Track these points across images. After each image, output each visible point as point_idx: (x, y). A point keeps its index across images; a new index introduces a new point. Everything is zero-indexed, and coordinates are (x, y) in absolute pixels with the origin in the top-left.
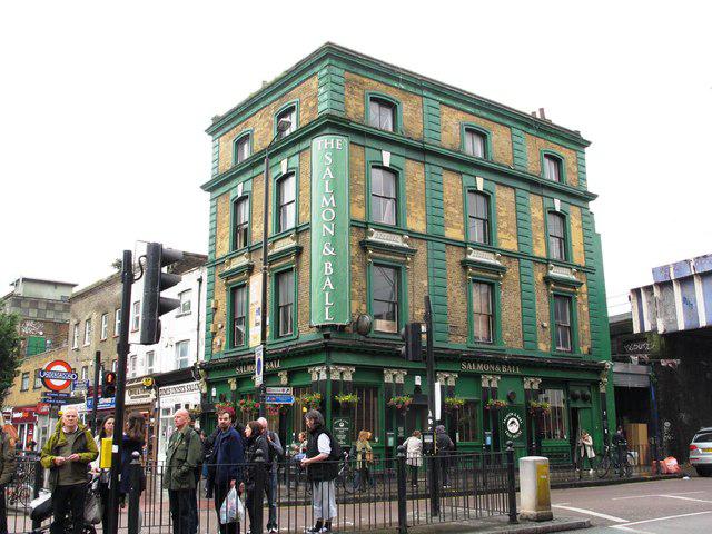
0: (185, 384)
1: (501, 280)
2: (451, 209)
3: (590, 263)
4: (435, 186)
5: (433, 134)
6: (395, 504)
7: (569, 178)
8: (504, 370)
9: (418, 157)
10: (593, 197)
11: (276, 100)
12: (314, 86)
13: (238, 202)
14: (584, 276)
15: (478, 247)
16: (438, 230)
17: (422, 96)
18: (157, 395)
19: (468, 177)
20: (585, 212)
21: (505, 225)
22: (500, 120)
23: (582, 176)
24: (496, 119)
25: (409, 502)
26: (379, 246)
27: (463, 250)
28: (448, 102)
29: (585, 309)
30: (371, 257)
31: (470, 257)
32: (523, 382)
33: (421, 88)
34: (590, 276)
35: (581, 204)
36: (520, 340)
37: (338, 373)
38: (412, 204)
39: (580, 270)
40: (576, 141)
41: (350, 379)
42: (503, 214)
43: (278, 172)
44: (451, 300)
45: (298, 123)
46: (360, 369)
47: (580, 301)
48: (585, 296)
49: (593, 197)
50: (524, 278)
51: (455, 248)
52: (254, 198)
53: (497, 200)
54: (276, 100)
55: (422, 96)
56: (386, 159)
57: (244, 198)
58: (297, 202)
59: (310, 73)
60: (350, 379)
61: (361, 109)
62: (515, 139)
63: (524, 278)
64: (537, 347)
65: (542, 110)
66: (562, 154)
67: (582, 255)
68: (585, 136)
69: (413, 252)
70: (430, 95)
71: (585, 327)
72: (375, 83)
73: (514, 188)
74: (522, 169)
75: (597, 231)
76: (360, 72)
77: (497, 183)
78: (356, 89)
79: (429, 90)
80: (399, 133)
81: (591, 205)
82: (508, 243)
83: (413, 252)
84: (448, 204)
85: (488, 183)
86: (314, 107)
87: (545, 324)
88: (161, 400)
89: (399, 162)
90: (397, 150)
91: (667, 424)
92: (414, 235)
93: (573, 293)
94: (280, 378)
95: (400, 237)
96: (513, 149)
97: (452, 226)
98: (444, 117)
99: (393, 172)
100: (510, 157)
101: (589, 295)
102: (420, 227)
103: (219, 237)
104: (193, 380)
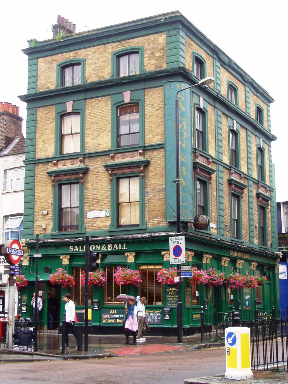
32: (250, 265)
40: (268, 100)
103: (38, 139)
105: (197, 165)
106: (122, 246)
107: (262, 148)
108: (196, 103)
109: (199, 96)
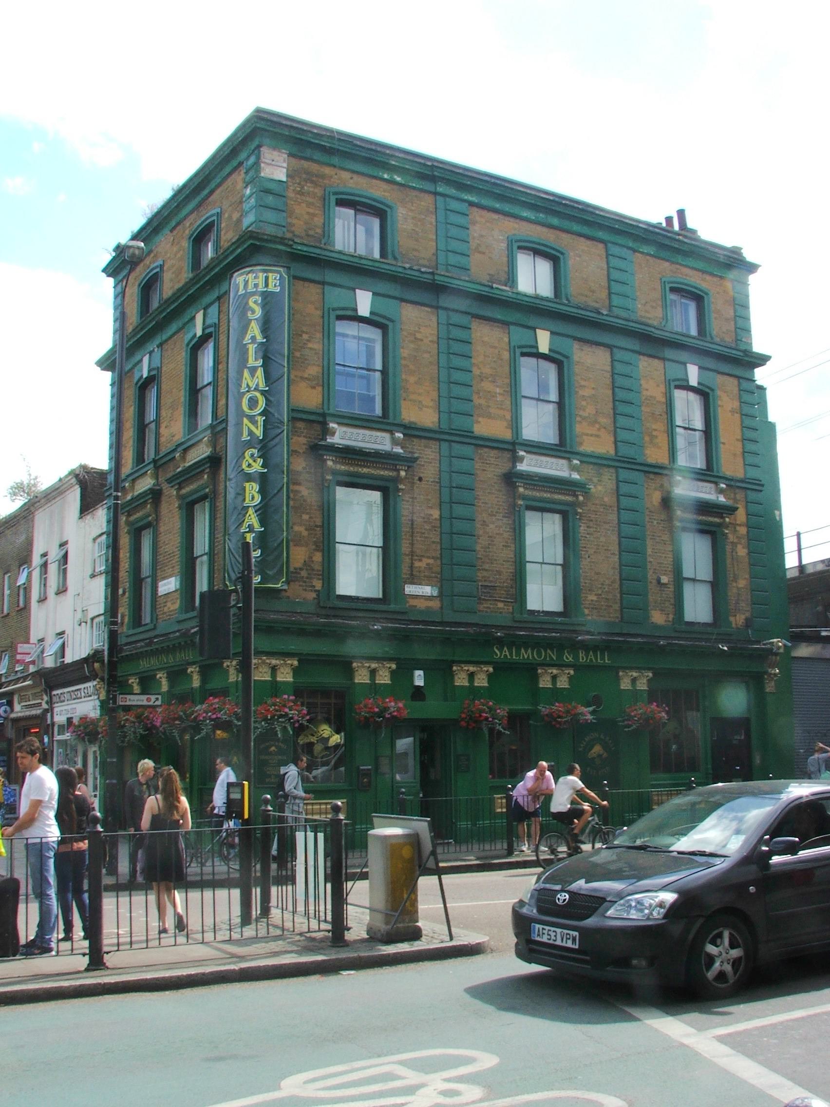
0: (81, 686)
1: (581, 505)
2: (487, 385)
3: (752, 473)
4: (456, 347)
5: (453, 259)
6: (236, 893)
7: (718, 328)
8: (582, 657)
9: (426, 297)
10: (762, 360)
11: (192, 212)
12: (240, 185)
13: (144, 386)
14: (740, 495)
15: (538, 448)
16: (459, 422)
17: (436, 194)
18: (50, 702)
19: (520, 329)
20: (745, 385)
21: (590, 410)
22: (585, 230)
23: (740, 323)
24: (576, 227)
25: (274, 890)
26: (531, 479)
27: (507, 455)
28: (485, 202)
29: (742, 552)
30: (524, 498)
31: (522, 467)
33: (433, 179)
34: (752, 496)
35: (738, 372)
36: (617, 606)
37: (549, 678)
38: (412, 379)
39: (734, 485)
41: (290, 679)
42: (586, 392)
43: (190, 336)
44: (483, 541)
45: (217, 248)
46: (306, 662)
47: (731, 538)
48: (743, 530)
49: (762, 360)
50: (625, 502)
51: (493, 453)
52: (164, 379)
53: (577, 369)
54: (192, 212)
55: (436, 194)
56: (364, 303)
57: (150, 380)
58: (215, 383)
59: (235, 163)
60: (290, 679)
61: (319, 221)
62: (614, 262)
63: (625, 502)
64: (647, 617)
65: (681, 213)
66: (704, 286)
67: (740, 460)
68: (749, 255)
69: (410, 462)
70: (452, 191)
71: (742, 583)
72: (346, 175)
73: (610, 347)
74: (623, 314)
75: (771, 419)
76: (317, 155)
77: (575, 339)
78: (308, 187)
79: (448, 182)
80: (709, 339)
81: (760, 375)
82: (603, 446)
83: (731, 510)
84: (482, 378)
85: (559, 339)
86: (239, 221)
87: (664, 579)
88: (56, 710)
89: (389, 308)
90: (385, 287)
91: (292, 772)
92: (412, 432)
93: (719, 525)
94: (190, 677)
95: (387, 436)
96: (609, 280)
97: (489, 416)
98: (476, 231)
99: (556, 359)
100: (604, 295)
101: (748, 527)
102: (427, 418)
104: (86, 679)
105: (515, 480)
106: (603, 658)
107: (700, 387)
108: (672, 378)
109: (685, 364)
